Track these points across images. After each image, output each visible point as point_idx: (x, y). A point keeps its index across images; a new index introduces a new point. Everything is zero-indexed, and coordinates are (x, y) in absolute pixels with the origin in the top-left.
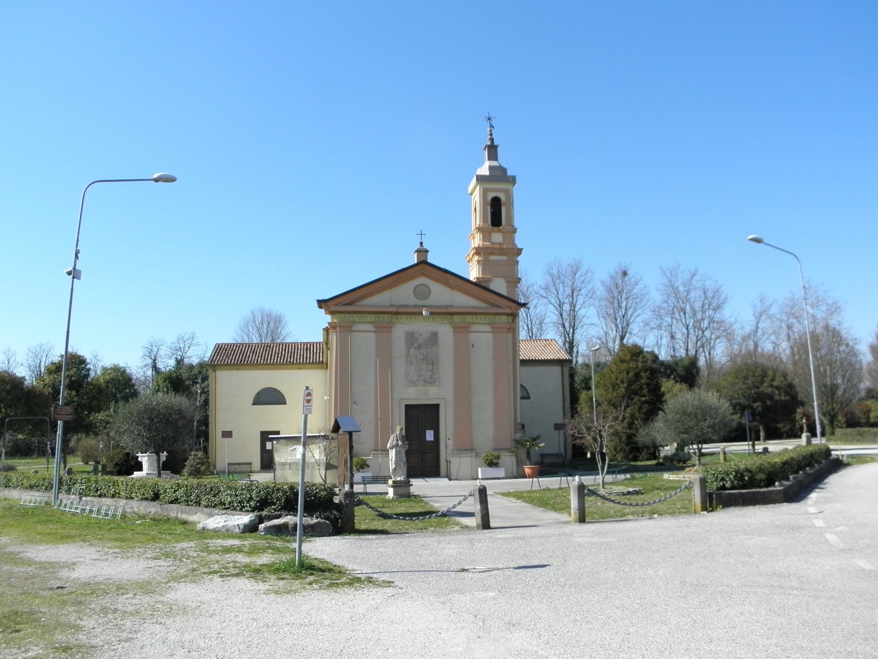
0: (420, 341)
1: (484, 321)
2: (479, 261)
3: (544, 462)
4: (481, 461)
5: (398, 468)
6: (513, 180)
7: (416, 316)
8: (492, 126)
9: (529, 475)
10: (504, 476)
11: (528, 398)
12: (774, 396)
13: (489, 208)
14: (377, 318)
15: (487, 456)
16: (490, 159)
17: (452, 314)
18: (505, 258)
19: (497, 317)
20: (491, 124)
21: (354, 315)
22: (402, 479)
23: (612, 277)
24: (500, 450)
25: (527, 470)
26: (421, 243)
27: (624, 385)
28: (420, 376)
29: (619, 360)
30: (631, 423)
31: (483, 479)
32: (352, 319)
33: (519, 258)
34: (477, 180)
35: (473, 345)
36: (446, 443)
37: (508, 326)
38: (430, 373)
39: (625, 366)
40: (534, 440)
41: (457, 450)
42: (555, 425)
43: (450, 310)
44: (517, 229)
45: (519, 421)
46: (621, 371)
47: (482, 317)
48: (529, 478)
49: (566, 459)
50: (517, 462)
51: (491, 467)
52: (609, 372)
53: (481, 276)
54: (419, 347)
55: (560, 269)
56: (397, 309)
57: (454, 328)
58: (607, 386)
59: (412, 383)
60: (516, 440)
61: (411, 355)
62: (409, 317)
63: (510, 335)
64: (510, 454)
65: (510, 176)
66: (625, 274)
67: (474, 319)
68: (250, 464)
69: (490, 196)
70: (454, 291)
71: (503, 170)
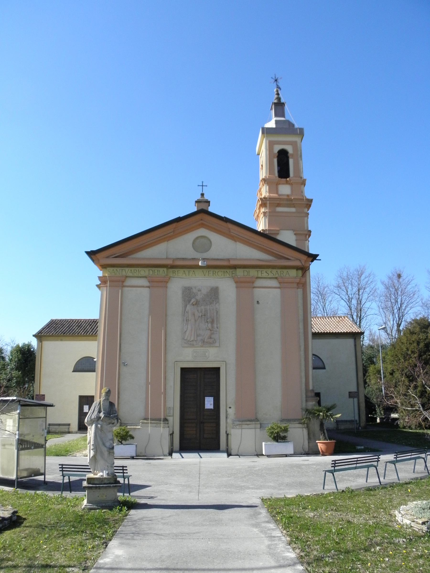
0: (199, 297)
1: (271, 275)
2: (265, 213)
3: (339, 428)
4: (265, 433)
5: (99, 457)
6: (301, 133)
7: (195, 270)
8: (278, 87)
9: (322, 451)
10: (292, 452)
11: (324, 368)
13: (276, 160)
14: (151, 272)
15: (273, 428)
16: (276, 115)
17: (235, 267)
18: (293, 210)
19: (285, 271)
20: (277, 86)
21: (127, 269)
22: (105, 476)
23: (390, 278)
24: (289, 421)
25: (321, 446)
26: (202, 195)
27: (415, 355)
28: (198, 336)
29: (408, 332)
30: (423, 391)
31: (269, 456)
32: (124, 273)
34: (263, 133)
35: (258, 302)
36: (227, 411)
37: (298, 280)
38: (208, 332)
39: (414, 337)
40: (328, 410)
41: (239, 421)
42: (350, 393)
43: (232, 263)
44: (305, 180)
45: (311, 388)
46: (411, 342)
47: (269, 271)
48: (324, 455)
49: (360, 426)
50: (309, 434)
51: (277, 441)
52: (400, 344)
53: (267, 228)
54: (197, 303)
55: (349, 273)
56: (173, 261)
58: (398, 357)
59: (189, 344)
60: (307, 410)
61: (187, 312)
62: (186, 270)
63: (300, 291)
64: (300, 425)
65: (297, 129)
66: (399, 276)
67: (260, 272)
68: (69, 425)
69: (277, 148)
70: (237, 243)
71: (290, 125)
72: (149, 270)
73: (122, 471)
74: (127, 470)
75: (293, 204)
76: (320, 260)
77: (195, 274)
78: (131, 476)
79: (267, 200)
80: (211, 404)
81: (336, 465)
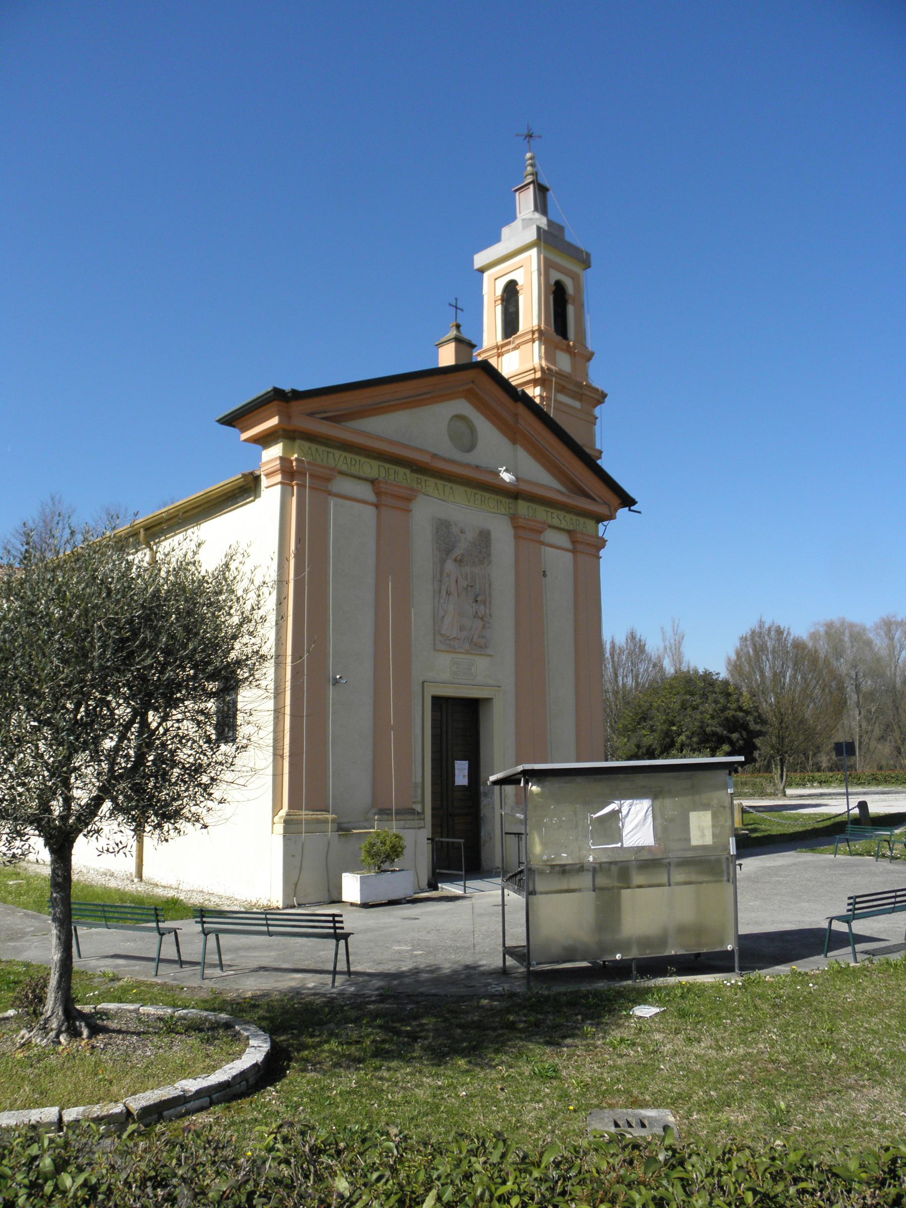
12: (748, 724)
13: (551, 297)
18: (578, 405)
32: (331, 463)
33: (597, 411)
57: (516, 528)
69: (555, 276)
72: (379, 466)
73: (331, 925)
74: (341, 922)
75: (582, 395)
76: (639, 512)
77: (453, 493)
78: (353, 934)
79: (553, 376)
80: (464, 776)
81: (857, 906)
